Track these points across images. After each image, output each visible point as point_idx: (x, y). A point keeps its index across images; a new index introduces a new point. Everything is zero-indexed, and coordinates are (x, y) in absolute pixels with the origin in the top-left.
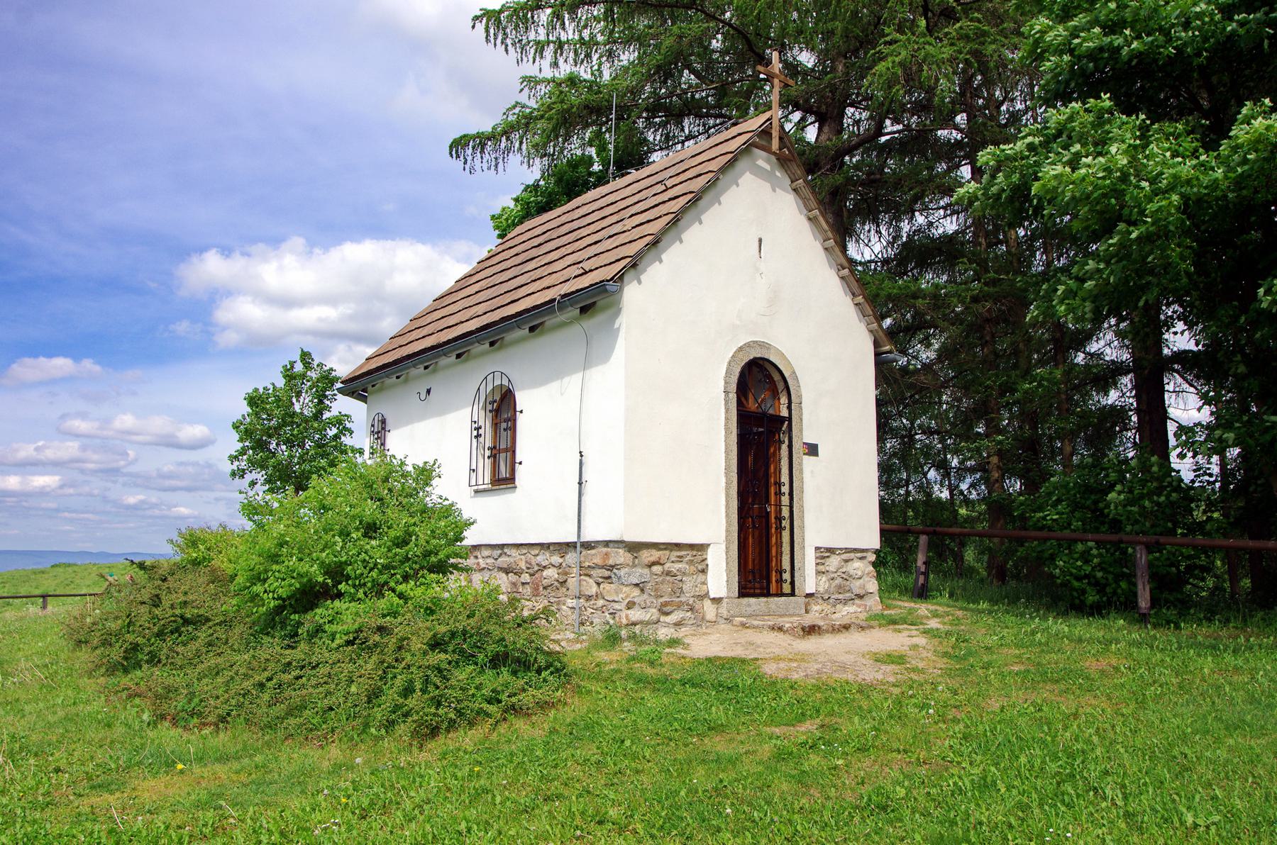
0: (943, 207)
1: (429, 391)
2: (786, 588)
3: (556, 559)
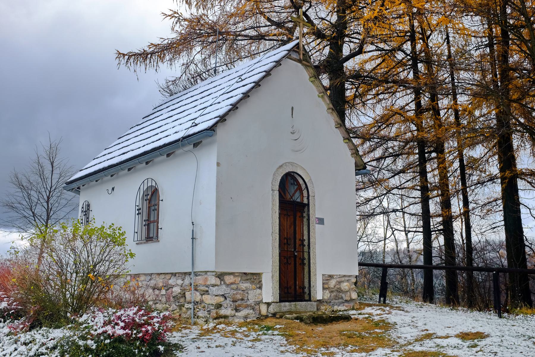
1: (113, 189)
2: (307, 297)
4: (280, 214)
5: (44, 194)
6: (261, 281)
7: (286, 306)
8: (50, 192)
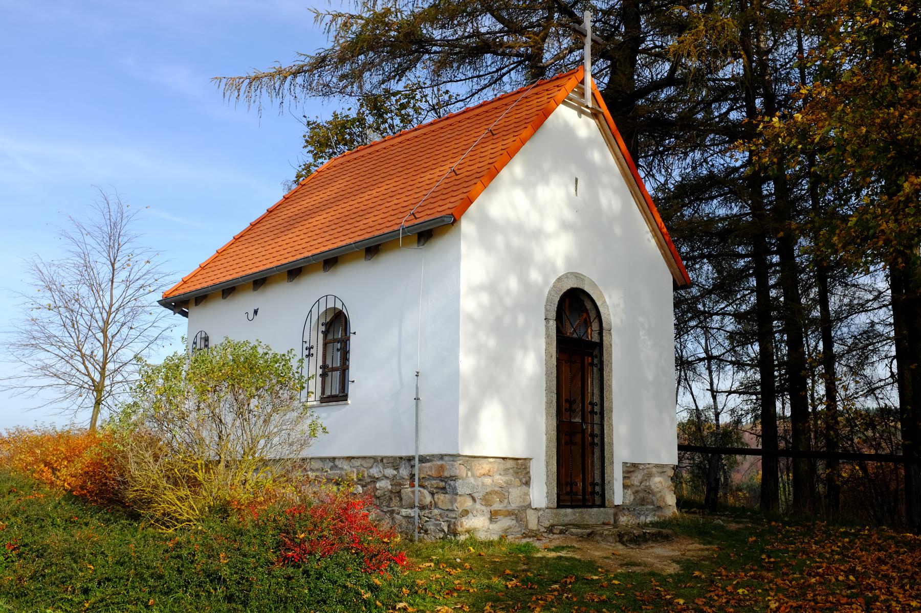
0: (455, 54)
1: (256, 312)
2: (598, 500)
3: (390, 472)
4: (558, 359)
5: (98, 316)
6: (529, 472)
7: (569, 514)
8: (109, 314)
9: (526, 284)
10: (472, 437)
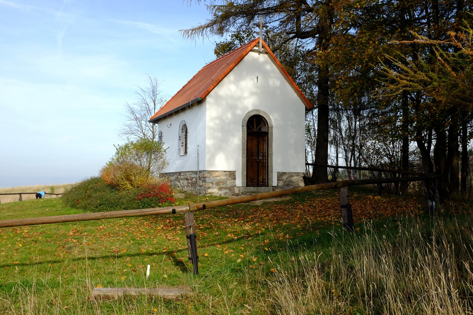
9: (234, 115)
10: (212, 164)
